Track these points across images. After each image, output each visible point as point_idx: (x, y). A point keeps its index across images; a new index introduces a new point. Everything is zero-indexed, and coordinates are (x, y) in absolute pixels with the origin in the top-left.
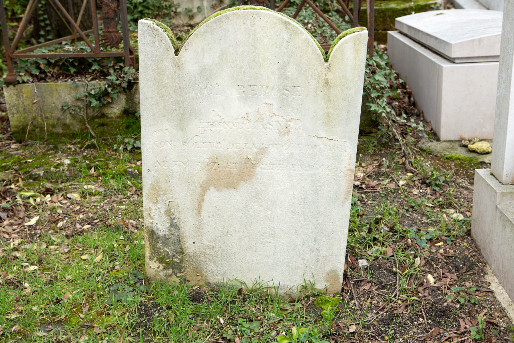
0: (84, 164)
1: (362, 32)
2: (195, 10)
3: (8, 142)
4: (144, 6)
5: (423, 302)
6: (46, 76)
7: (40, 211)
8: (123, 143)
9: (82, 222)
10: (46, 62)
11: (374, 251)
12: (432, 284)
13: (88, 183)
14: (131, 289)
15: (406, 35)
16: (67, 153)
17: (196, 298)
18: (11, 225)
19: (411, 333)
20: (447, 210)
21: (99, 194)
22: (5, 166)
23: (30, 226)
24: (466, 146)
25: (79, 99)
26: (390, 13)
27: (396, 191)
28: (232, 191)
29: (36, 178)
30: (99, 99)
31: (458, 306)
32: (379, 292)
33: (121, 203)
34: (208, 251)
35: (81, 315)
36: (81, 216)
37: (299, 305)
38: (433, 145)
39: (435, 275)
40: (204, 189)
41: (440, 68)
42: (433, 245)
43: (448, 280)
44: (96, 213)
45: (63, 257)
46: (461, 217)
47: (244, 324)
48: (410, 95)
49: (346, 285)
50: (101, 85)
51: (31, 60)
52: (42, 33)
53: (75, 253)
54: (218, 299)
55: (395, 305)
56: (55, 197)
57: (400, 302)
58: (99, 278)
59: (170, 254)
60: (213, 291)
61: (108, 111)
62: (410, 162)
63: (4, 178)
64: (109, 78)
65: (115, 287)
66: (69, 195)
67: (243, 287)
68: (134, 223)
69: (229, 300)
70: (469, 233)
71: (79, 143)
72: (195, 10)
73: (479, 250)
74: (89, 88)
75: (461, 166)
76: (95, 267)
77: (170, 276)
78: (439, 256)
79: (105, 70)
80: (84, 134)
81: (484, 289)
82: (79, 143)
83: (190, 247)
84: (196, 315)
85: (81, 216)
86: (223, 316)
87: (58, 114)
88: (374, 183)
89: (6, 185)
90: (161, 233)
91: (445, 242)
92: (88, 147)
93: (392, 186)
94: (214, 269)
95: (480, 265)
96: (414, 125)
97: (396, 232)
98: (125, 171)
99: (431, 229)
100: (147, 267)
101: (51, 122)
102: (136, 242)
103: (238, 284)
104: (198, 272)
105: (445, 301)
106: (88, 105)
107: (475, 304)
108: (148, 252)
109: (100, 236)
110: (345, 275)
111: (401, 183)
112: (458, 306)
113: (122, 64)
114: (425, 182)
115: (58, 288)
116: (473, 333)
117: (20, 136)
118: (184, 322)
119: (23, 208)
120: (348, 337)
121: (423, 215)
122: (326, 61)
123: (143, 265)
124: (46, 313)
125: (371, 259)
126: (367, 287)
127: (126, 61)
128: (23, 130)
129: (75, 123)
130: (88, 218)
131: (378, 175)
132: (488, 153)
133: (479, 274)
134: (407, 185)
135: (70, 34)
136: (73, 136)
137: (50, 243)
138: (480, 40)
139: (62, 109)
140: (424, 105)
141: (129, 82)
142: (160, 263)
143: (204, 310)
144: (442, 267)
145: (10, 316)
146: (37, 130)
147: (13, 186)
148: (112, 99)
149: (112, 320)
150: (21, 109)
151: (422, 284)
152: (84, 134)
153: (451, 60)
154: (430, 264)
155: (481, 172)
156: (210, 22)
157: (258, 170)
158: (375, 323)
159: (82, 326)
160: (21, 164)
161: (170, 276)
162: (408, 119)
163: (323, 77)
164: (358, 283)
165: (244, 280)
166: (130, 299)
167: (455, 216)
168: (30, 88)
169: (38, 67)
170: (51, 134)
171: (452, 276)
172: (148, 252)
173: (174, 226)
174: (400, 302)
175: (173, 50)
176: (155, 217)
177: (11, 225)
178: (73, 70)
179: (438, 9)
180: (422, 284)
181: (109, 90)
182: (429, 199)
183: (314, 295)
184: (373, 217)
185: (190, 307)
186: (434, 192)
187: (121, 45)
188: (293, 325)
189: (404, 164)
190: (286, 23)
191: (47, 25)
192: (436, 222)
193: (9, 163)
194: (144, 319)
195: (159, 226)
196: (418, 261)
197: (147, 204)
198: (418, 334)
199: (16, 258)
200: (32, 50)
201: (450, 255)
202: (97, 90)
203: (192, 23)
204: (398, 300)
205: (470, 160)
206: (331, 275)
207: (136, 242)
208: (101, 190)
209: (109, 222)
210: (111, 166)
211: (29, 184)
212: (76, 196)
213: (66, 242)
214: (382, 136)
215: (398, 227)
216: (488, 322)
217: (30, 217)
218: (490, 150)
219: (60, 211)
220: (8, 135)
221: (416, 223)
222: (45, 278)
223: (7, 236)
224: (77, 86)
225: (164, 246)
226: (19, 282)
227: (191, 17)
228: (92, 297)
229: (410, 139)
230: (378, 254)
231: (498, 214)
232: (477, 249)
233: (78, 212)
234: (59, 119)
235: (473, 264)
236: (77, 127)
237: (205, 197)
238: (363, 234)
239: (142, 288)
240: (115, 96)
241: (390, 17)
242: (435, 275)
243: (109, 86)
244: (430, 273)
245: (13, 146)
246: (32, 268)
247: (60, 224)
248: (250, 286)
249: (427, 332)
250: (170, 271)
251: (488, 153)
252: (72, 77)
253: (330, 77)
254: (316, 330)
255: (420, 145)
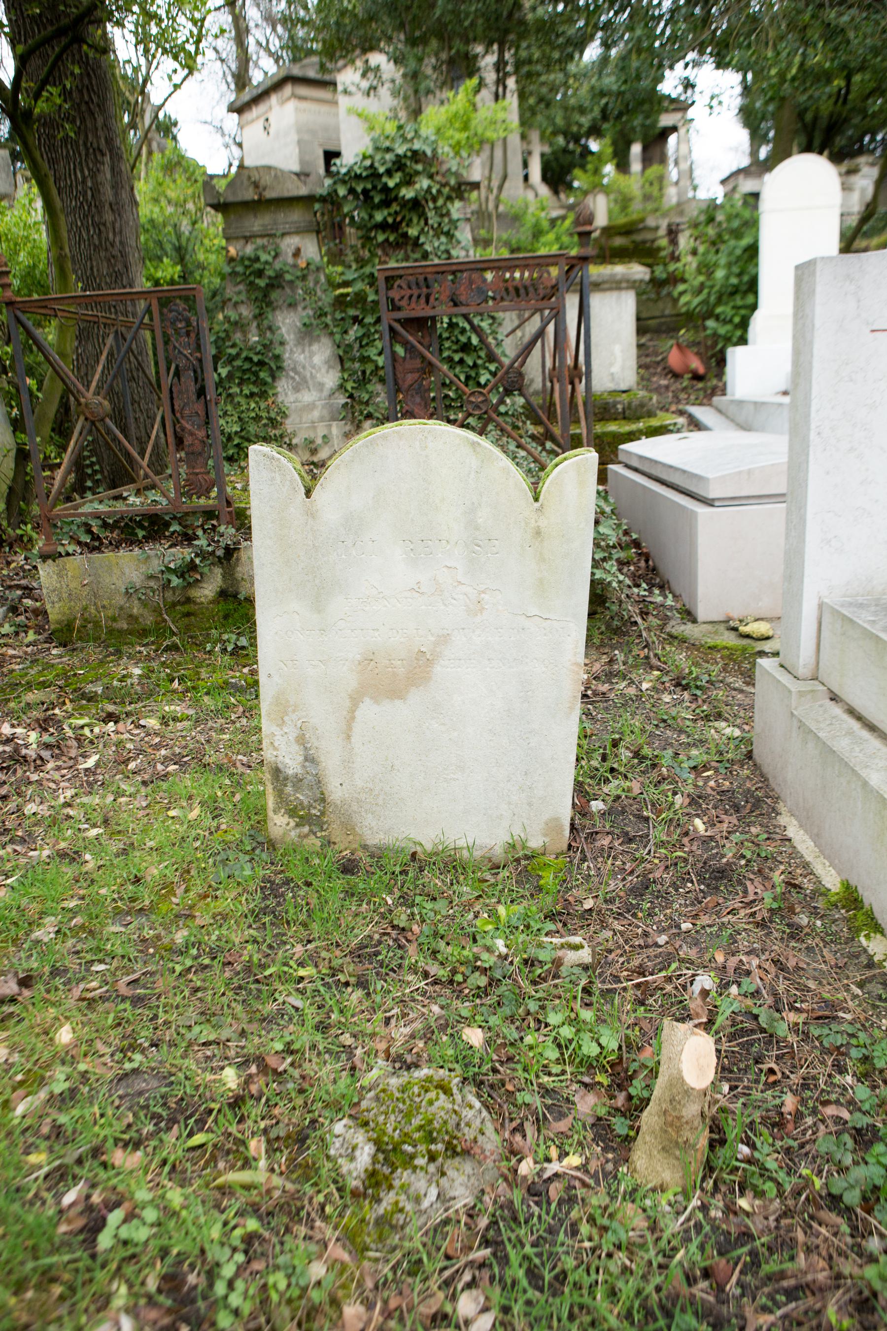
0: (163, 675)
1: (589, 455)
2: (319, 441)
3: (47, 645)
4: (242, 438)
5: (691, 859)
6: (102, 544)
7: (101, 746)
8: (220, 640)
9: (166, 761)
10: (100, 522)
11: (613, 787)
12: (703, 833)
13: (171, 702)
14: (247, 858)
15: (636, 470)
16: (136, 659)
17: (349, 868)
18: (58, 768)
19: (676, 906)
20: (716, 724)
21: (188, 718)
22: (44, 682)
23: (86, 770)
24: (735, 629)
25: (151, 577)
26: (609, 439)
27: (639, 697)
28: (398, 702)
29: (92, 698)
30: (182, 576)
31: (743, 862)
32: (624, 848)
33: (222, 731)
34: (363, 796)
35: (174, 900)
36: (163, 752)
37: (505, 873)
38: (688, 630)
39: (705, 819)
40: (355, 701)
41: (693, 515)
42: (698, 775)
43: (725, 825)
44: (185, 747)
45: (141, 814)
46: (737, 733)
47: (425, 904)
48: (647, 557)
49: (575, 840)
50: (183, 554)
51: (78, 520)
52: (89, 484)
53: (157, 807)
54: (381, 867)
55: (649, 866)
56: (121, 725)
57: (656, 861)
58: (198, 844)
59: (306, 803)
60: (372, 856)
61: (195, 593)
62: (656, 655)
63: (43, 699)
64: (196, 542)
65: (223, 856)
66: (142, 722)
67: (419, 849)
68: (245, 759)
69: (398, 869)
70: (749, 755)
71: (153, 643)
72: (319, 441)
73: (767, 780)
74: (167, 559)
75: (730, 657)
76: (190, 827)
77: (306, 836)
78: (709, 791)
79: (190, 532)
80: (160, 630)
81: (778, 837)
82: (153, 643)
83: (336, 791)
84: (349, 893)
85: (163, 752)
86: (391, 893)
87: (120, 600)
88: (605, 688)
89: (47, 710)
90: (290, 772)
91: (716, 770)
92: (168, 649)
93: (632, 691)
94: (374, 824)
95: (769, 801)
96: (659, 599)
97: (645, 758)
98: (226, 683)
99: (694, 752)
100: (270, 824)
101: (110, 613)
102: (249, 788)
103: (411, 845)
104: (349, 828)
105: (723, 856)
106: (167, 585)
107: (766, 858)
108: (271, 801)
109: (194, 780)
110: (572, 826)
111: (645, 686)
112: (743, 862)
113: (215, 522)
114: (680, 684)
115: (137, 860)
116: (768, 901)
117: (65, 636)
118: (334, 904)
119: (75, 744)
120: (582, 917)
121: (681, 731)
122: (536, 500)
123: (262, 823)
124: (121, 899)
125: (610, 800)
126: (606, 841)
127: (222, 517)
128: (69, 626)
129: (146, 612)
130: (174, 755)
131: (610, 676)
132: (768, 638)
133: (769, 815)
134: (654, 688)
135: (133, 481)
136: (144, 633)
137: (119, 794)
138: (749, 472)
139: (127, 592)
140: (669, 570)
141: (227, 548)
142: (291, 816)
143: (361, 886)
144: (715, 807)
145: (65, 904)
146: (90, 626)
147: (57, 711)
148: (201, 575)
149: (222, 905)
150: (65, 595)
151: (686, 834)
152: (160, 630)
153: (709, 502)
154: (697, 803)
155: (764, 663)
156: (347, 454)
157: (437, 669)
158: (622, 894)
159: (176, 916)
160: (67, 678)
161: (306, 836)
162: (650, 591)
163: (533, 524)
164: (592, 836)
165: (419, 838)
166: (247, 872)
167: (728, 731)
168: (77, 563)
169: (89, 531)
170: (111, 631)
171: (730, 820)
172: (271, 801)
173: (310, 759)
174: (656, 861)
175: (303, 490)
176: (280, 747)
177: (58, 768)
178: (141, 533)
179: (678, 431)
180: (686, 834)
181: (197, 561)
182: (688, 708)
183: (527, 858)
184: (608, 738)
185: (340, 883)
186: (695, 698)
187: (213, 494)
188: (499, 902)
189: (647, 657)
190: (474, 444)
191: (95, 472)
192: (701, 741)
193: (50, 677)
194: (271, 902)
195: (287, 760)
196: (679, 799)
197: (267, 726)
198: (686, 906)
199: (69, 817)
200: (76, 508)
201: (725, 788)
202: (179, 562)
203: (316, 459)
204: (654, 860)
205: (742, 653)
206: (552, 826)
207: (249, 788)
208: (191, 712)
209: (206, 760)
210: (204, 675)
211: (82, 707)
212: (152, 723)
213: (143, 791)
214: (612, 618)
215: (646, 751)
216: (788, 884)
217: (85, 756)
218: (770, 633)
219: (130, 746)
220: (46, 635)
221: (671, 744)
222: (115, 846)
223: (53, 786)
224: (148, 557)
225: (296, 791)
226: (76, 852)
227: (314, 452)
228: (188, 872)
229: (654, 621)
230: (619, 792)
231: (795, 724)
232: (764, 778)
233: (157, 747)
234: (121, 608)
235: (759, 800)
236: (149, 620)
237: (357, 713)
238: (594, 763)
239: (264, 856)
240: (206, 570)
241: (609, 444)
242: (705, 819)
243: (197, 555)
244: (698, 816)
245: (54, 652)
246: (94, 832)
247: (132, 766)
248: (429, 847)
249: (700, 902)
250: (306, 829)
251: (768, 638)
252: (139, 543)
253: (543, 523)
254: (534, 908)
255: (668, 629)
